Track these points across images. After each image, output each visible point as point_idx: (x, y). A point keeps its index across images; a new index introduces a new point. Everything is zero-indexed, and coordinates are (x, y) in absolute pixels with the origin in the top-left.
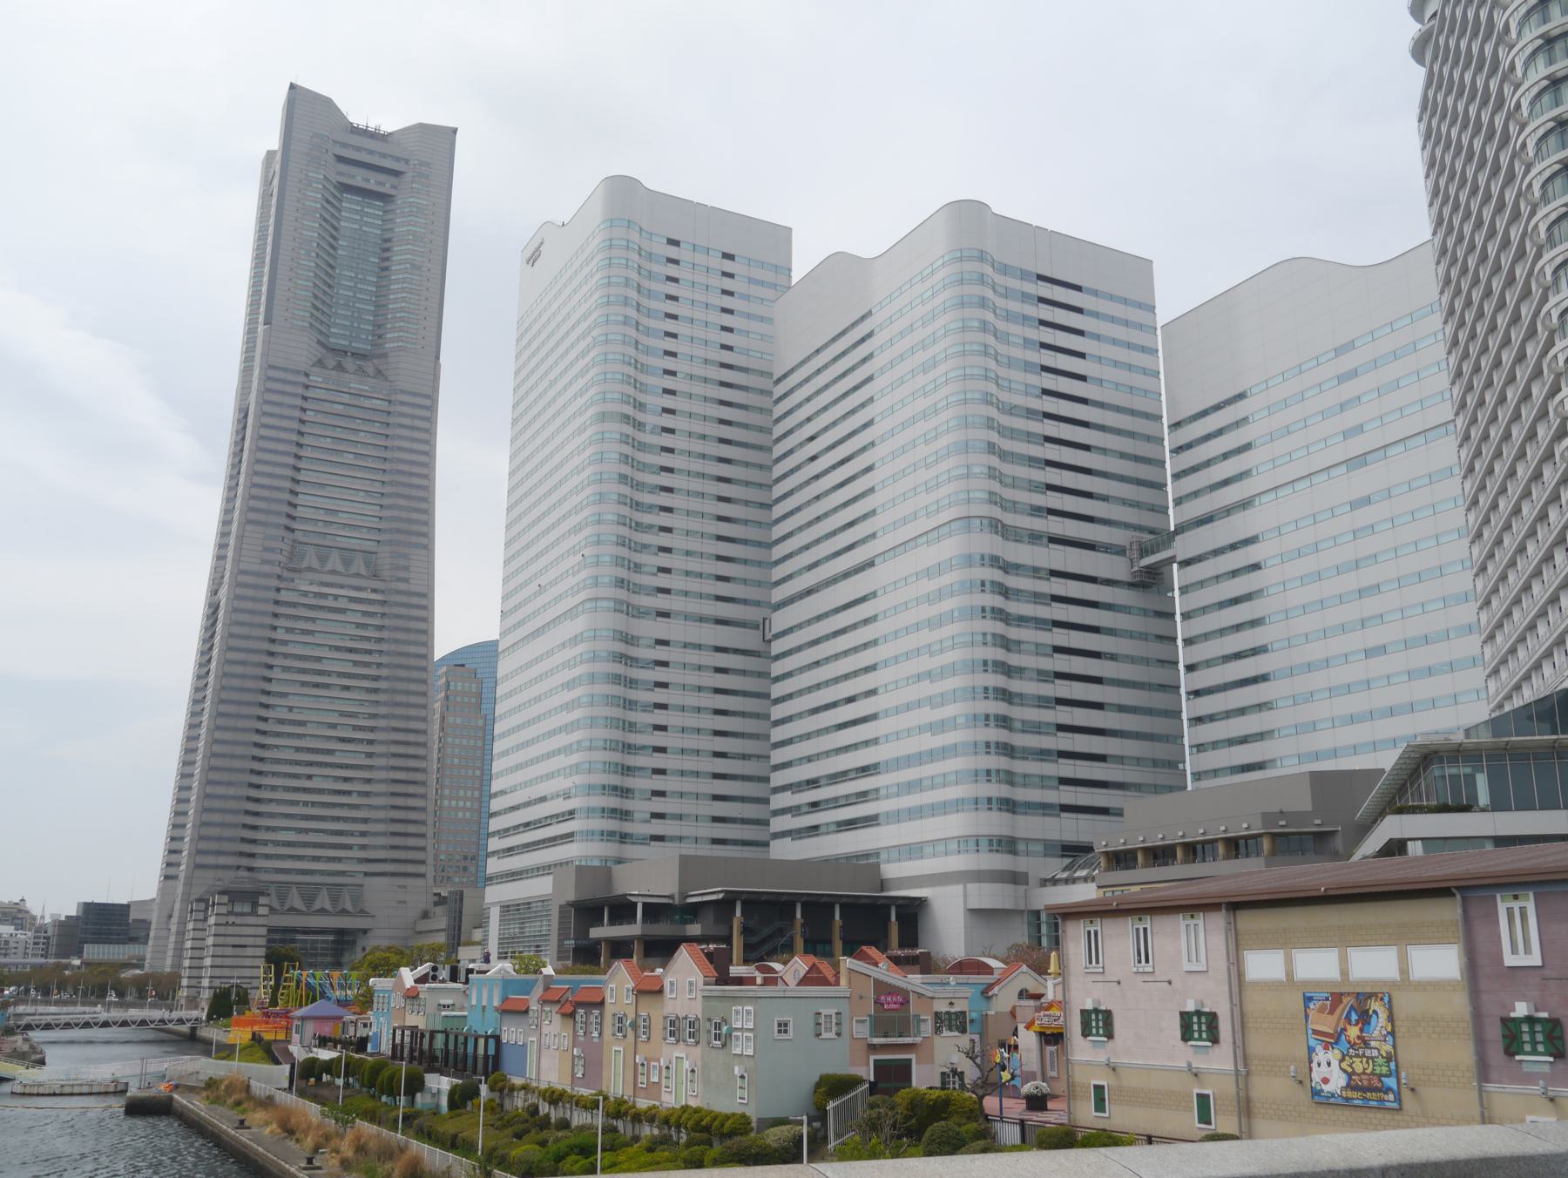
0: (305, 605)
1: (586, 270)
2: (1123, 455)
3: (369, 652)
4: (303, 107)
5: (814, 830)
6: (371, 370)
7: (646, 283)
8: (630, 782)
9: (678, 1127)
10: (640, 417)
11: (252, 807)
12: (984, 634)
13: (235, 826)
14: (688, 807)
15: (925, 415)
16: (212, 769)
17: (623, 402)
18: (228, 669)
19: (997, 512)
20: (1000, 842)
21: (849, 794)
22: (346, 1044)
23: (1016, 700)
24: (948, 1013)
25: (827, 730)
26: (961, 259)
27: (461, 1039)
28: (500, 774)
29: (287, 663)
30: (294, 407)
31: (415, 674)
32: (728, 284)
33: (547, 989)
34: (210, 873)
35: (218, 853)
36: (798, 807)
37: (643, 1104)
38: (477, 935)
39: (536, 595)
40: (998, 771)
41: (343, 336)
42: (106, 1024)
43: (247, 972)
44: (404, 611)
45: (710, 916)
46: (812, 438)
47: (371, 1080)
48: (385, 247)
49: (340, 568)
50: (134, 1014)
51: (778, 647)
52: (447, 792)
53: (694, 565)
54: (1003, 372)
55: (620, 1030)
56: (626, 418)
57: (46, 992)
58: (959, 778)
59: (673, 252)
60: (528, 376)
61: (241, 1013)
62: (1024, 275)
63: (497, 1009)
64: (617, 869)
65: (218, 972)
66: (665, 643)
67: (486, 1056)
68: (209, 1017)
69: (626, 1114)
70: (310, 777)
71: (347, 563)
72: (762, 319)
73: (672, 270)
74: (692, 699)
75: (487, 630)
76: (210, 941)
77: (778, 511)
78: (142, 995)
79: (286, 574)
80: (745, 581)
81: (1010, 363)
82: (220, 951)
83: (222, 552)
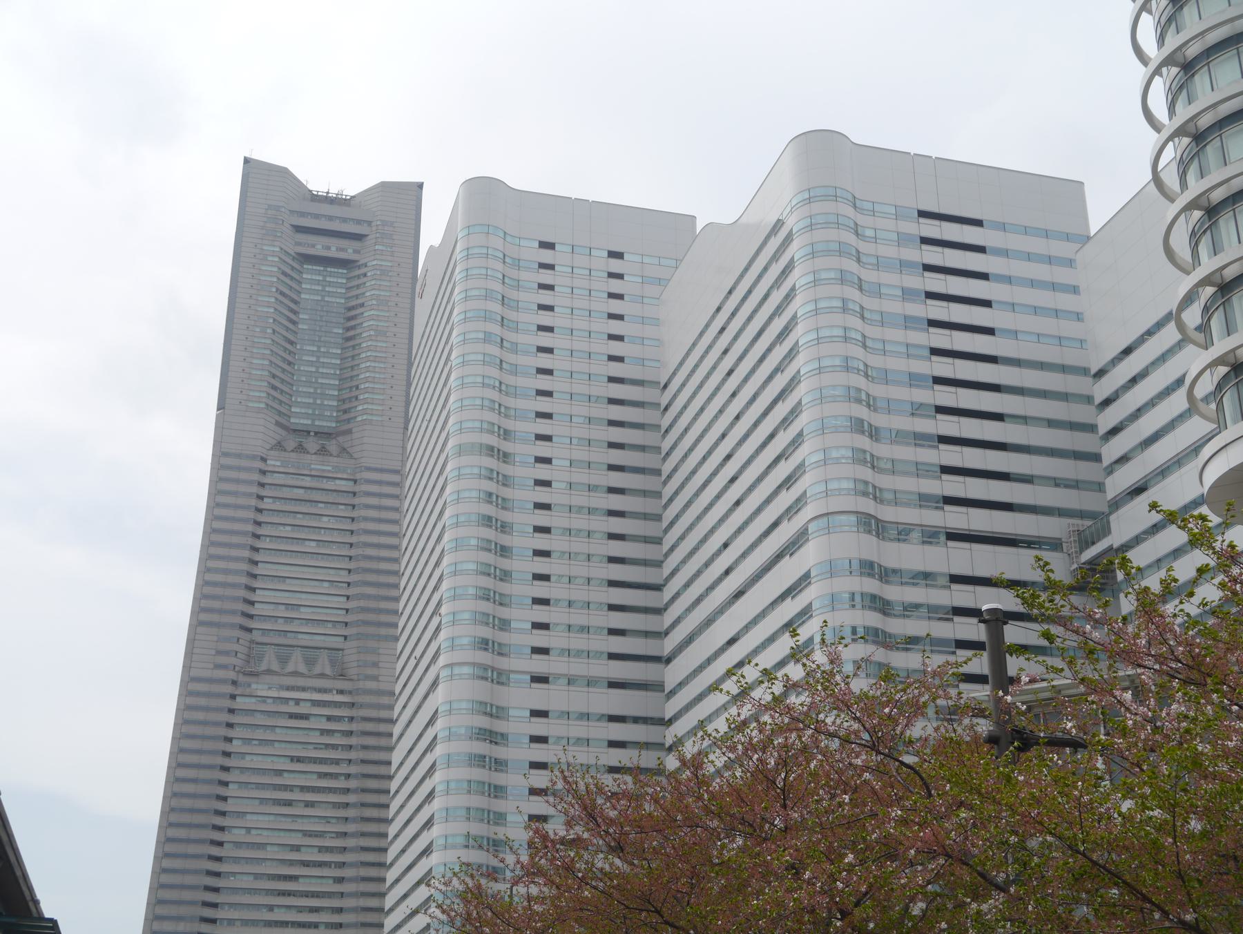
2: (1052, 423)
3: (337, 762)
4: (262, 181)
17: (857, 493)
19: (868, 506)
41: (307, 416)
48: (351, 316)
49: (302, 668)
54: (873, 332)
56: (491, 450)
66: (542, 714)
70: (271, 908)
71: (310, 662)
81: (884, 320)
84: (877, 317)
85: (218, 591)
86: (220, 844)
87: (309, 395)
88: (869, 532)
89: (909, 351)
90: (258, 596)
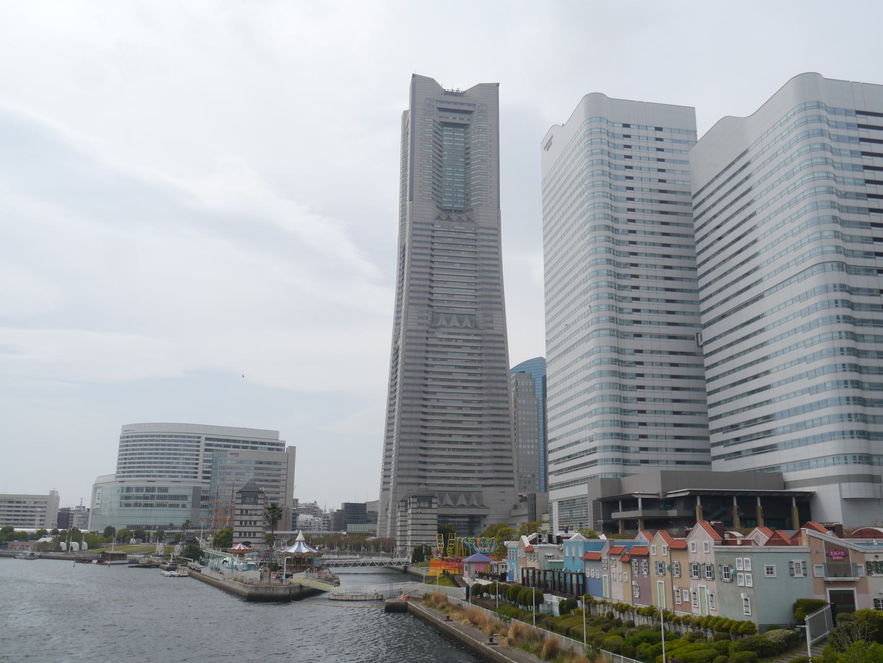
0: (441, 345)
1: (578, 149)
4: (421, 86)
5: (738, 454)
6: (465, 219)
7: (612, 151)
8: (626, 431)
9: (706, 627)
10: (616, 226)
11: (423, 452)
12: (840, 332)
13: (415, 462)
14: (661, 444)
15: (789, 205)
16: (402, 433)
17: (605, 218)
18: (406, 381)
19: (842, 258)
20: (860, 458)
21: (758, 433)
22: (494, 577)
23: (864, 371)
24: (875, 562)
25: (742, 395)
26: (805, 109)
27: (562, 575)
28: (552, 430)
29: (435, 376)
30: (428, 242)
31: (501, 378)
32: (660, 145)
33: (611, 547)
34: (405, 487)
35: (408, 476)
36: (727, 441)
37: (680, 614)
38: (546, 517)
39: (565, 330)
40: (856, 414)
41: (449, 202)
42: (364, 565)
43: (429, 538)
44: (492, 345)
45: (681, 505)
46: (718, 227)
47: (519, 598)
49: (457, 324)
50: (374, 559)
51: (707, 349)
52: (520, 440)
53: (653, 306)
54: (839, 173)
55: (661, 571)
56: (608, 228)
57: (332, 547)
58: (830, 419)
59: (626, 131)
60: (550, 211)
61: (429, 559)
62: (847, 112)
63: (581, 558)
64: (623, 479)
65: (415, 538)
66: (640, 351)
67: (578, 585)
68: (413, 562)
69: (671, 619)
70: (450, 435)
71: (461, 321)
72: (682, 162)
73: (627, 142)
74: (658, 382)
75: (539, 351)
76: (410, 522)
77: (701, 271)
78: (377, 549)
79: (431, 330)
80: (684, 313)
81: (843, 167)
82: (415, 527)
83: (398, 321)
84: (839, 166)
85: (417, 288)
86: (426, 406)
87: (450, 192)
88: (843, 270)
89: (855, 182)
90: (434, 290)
